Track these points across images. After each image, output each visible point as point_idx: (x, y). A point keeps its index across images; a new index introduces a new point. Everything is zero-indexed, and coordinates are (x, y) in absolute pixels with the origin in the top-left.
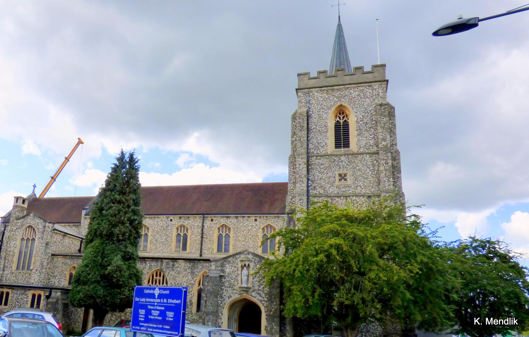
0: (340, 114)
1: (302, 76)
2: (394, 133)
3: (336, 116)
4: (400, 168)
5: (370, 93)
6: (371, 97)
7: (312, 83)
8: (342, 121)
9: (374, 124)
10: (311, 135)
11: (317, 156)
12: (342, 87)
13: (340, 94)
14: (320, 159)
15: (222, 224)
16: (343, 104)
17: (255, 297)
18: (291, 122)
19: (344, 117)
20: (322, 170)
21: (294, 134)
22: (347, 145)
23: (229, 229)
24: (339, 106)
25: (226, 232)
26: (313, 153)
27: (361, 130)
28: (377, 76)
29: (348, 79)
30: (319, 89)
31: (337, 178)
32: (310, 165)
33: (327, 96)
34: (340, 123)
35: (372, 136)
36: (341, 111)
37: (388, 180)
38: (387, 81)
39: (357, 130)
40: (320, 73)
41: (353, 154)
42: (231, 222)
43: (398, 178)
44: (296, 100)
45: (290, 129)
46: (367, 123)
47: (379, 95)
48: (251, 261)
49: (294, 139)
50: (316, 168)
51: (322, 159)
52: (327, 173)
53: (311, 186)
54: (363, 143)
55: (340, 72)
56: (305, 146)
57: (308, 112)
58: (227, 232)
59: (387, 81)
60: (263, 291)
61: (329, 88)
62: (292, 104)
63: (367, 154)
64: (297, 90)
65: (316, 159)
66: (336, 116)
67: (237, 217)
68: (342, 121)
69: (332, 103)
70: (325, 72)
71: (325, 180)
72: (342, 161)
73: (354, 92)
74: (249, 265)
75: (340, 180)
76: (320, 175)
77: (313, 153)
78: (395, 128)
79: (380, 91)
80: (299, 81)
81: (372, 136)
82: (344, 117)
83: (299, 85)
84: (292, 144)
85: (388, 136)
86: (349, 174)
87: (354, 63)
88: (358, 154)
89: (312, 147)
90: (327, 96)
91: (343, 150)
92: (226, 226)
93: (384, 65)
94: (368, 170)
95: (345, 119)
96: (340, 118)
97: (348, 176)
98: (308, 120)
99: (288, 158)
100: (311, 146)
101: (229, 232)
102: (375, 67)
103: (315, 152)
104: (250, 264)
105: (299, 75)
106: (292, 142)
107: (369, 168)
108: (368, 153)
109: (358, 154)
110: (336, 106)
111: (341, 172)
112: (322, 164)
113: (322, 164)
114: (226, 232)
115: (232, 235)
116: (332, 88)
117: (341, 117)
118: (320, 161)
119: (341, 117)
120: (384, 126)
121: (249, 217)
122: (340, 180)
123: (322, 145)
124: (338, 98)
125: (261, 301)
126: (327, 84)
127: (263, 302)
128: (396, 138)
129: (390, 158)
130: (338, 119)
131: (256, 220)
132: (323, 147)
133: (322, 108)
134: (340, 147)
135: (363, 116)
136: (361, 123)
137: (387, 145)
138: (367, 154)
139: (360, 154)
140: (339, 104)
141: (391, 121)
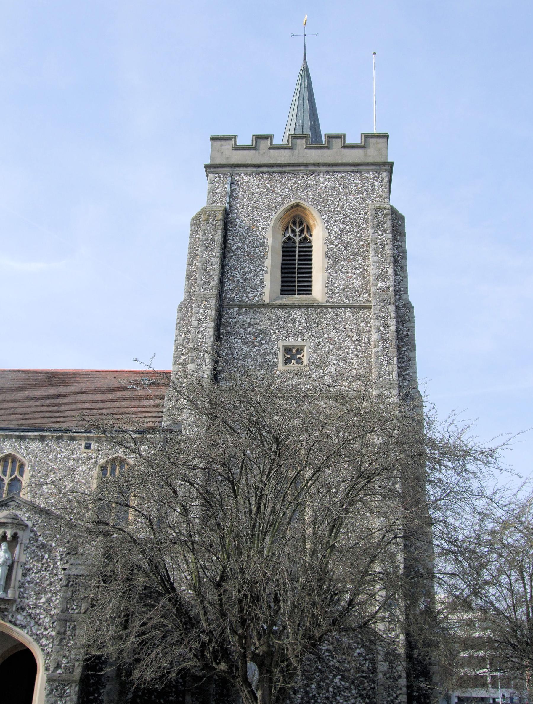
0: (294, 223)
1: (220, 143)
2: (402, 267)
3: (287, 229)
4: (413, 340)
5: (357, 185)
6: (361, 193)
7: (239, 157)
8: (297, 239)
9: (362, 246)
10: (231, 262)
11: (240, 307)
12: (302, 168)
13: (296, 182)
14: (247, 314)
15: (6, 452)
16: (302, 202)
17: (23, 627)
18: (188, 233)
19: (302, 231)
20: (250, 338)
21: (193, 257)
22: (306, 287)
23: (22, 467)
24: (293, 207)
25: (13, 472)
26: (232, 299)
27: (336, 257)
28: (372, 154)
29: (314, 156)
30: (254, 169)
31: (293, 366)
32: (225, 326)
33: (268, 185)
34: (294, 242)
35: (358, 271)
36: (296, 219)
37: (389, 363)
38: (391, 165)
39: (328, 257)
40: (258, 138)
41: (318, 306)
42: (27, 449)
43: (409, 360)
44: (206, 186)
45: (187, 246)
46: (348, 245)
47: (373, 190)
48: (23, 526)
49: (193, 269)
50: (237, 332)
51: (251, 313)
52: (261, 345)
53: (223, 371)
54: (340, 283)
55: (298, 141)
56: (215, 282)
57: (226, 213)
58: (16, 474)
59: (391, 165)
60: (47, 611)
61: (275, 169)
62: (197, 194)
63: (346, 307)
64: (207, 167)
65: (239, 314)
66: (287, 229)
67: (42, 439)
68: (297, 239)
69: (280, 199)
70: (269, 138)
71: (254, 359)
72: (294, 321)
73: (325, 182)
74: (15, 537)
75: (287, 361)
76: (245, 349)
77: (232, 299)
78: (405, 257)
79: (377, 184)
80: (212, 150)
81: (358, 271)
82: (302, 231)
83: (212, 159)
84: (188, 279)
85: (391, 272)
86: (308, 346)
87: (326, 128)
88: (327, 307)
89: (232, 287)
90: (268, 185)
91: (297, 298)
92: (14, 459)
93: (385, 136)
94: (348, 340)
95: (305, 234)
96: (293, 231)
97: (305, 352)
98: (225, 230)
99: (176, 309)
100: (229, 285)
101: (21, 474)
102: (367, 136)
103: (237, 299)
104: (20, 533)
105: (214, 139)
106: (189, 275)
107: (351, 337)
108: (351, 307)
109: (327, 307)
110: (288, 205)
111: (291, 342)
112: (250, 325)
113: (250, 325)
114: (13, 472)
115: (25, 479)
116: (280, 169)
117: (297, 230)
118: (247, 319)
119: (297, 230)
120: (384, 250)
121: (72, 439)
122: (287, 361)
123: (253, 285)
124: (291, 189)
125: (38, 638)
126: (271, 161)
127: (44, 642)
128: (406, 277)
129: (393, 315)
130: (290, 233)
131: (88, 446)
132: (255, 288)
133: (257, 208)
134: (292, 292)
135: (342, 231)
136: (336, 242)
137: (387, 288)
138: (346, 307)
139: (332, 307)
140: (293, 201)
141: (396, 244)
